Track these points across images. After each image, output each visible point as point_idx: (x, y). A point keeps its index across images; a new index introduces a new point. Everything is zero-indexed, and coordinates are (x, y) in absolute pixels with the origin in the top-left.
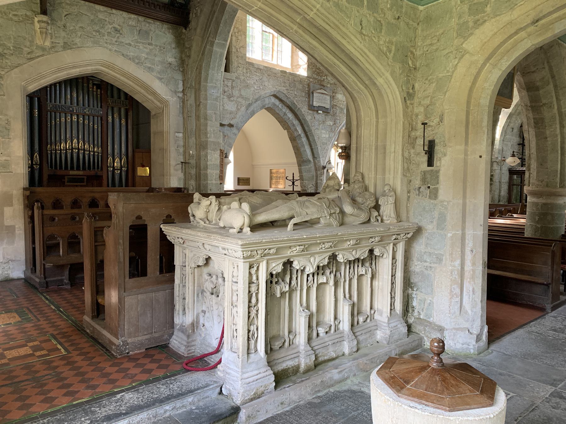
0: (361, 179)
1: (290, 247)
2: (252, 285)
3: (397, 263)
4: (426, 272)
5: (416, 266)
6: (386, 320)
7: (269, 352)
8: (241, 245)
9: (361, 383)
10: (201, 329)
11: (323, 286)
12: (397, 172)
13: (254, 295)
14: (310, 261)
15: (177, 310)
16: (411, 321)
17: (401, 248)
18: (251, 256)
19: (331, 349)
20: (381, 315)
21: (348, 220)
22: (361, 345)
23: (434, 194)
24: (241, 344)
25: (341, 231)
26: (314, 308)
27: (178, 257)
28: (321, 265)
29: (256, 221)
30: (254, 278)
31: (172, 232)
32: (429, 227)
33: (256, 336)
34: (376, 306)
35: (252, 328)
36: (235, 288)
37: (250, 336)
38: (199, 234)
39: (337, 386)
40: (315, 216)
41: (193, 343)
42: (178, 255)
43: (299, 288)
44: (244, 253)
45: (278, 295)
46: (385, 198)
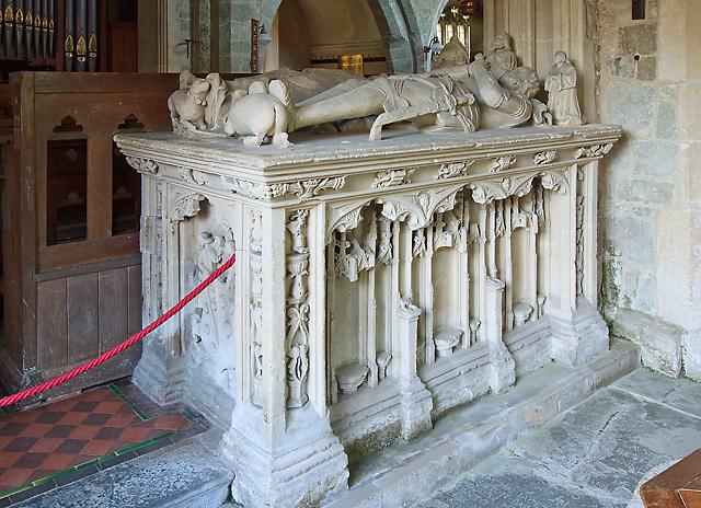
0: (507, 46)
1: (376, 174)
2: (295, 259)
3: (585, 203)
4: (638, 219)
5: (619, 209)
6: (569, 317)
7: (335, 399)
8: (265, 170)
9: (532, 457)
10: (194, 348)
11: (444, 253)
12: (576, 32)
13: (299, 279)
14: (418, 204)
15: (148, 308)
16: (612, 314)
17: (591, 171)
18: (289, 195)
19: (464, 382)
20: (558, 305)
21: (492, 118)
22: (522, 371)
23: (649, 71)
24: (270, 390)
25: (482, 140)
26: (427, 299)
27: (148, 202)
28: (442, 211)
29: (301, 119)
30: (299, 242)
31: (140, 150)
32: (642, 134)
33: (304, 369)
34: (546, 289)
35: (295, 353)
36: (256, 266)
37: (292, 371)
38: (180, 149)
39: (483, 464)
40: (427, 110)
41: (179, 377)
42: (148, 202)
43: (396, 260)
44: (273, 187)
45: (353, 277)
46: (558, 78)
